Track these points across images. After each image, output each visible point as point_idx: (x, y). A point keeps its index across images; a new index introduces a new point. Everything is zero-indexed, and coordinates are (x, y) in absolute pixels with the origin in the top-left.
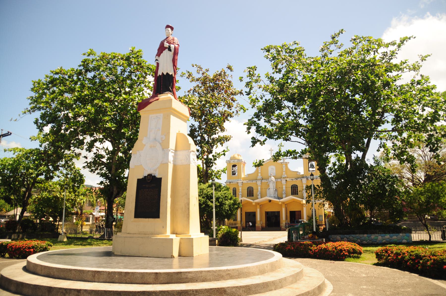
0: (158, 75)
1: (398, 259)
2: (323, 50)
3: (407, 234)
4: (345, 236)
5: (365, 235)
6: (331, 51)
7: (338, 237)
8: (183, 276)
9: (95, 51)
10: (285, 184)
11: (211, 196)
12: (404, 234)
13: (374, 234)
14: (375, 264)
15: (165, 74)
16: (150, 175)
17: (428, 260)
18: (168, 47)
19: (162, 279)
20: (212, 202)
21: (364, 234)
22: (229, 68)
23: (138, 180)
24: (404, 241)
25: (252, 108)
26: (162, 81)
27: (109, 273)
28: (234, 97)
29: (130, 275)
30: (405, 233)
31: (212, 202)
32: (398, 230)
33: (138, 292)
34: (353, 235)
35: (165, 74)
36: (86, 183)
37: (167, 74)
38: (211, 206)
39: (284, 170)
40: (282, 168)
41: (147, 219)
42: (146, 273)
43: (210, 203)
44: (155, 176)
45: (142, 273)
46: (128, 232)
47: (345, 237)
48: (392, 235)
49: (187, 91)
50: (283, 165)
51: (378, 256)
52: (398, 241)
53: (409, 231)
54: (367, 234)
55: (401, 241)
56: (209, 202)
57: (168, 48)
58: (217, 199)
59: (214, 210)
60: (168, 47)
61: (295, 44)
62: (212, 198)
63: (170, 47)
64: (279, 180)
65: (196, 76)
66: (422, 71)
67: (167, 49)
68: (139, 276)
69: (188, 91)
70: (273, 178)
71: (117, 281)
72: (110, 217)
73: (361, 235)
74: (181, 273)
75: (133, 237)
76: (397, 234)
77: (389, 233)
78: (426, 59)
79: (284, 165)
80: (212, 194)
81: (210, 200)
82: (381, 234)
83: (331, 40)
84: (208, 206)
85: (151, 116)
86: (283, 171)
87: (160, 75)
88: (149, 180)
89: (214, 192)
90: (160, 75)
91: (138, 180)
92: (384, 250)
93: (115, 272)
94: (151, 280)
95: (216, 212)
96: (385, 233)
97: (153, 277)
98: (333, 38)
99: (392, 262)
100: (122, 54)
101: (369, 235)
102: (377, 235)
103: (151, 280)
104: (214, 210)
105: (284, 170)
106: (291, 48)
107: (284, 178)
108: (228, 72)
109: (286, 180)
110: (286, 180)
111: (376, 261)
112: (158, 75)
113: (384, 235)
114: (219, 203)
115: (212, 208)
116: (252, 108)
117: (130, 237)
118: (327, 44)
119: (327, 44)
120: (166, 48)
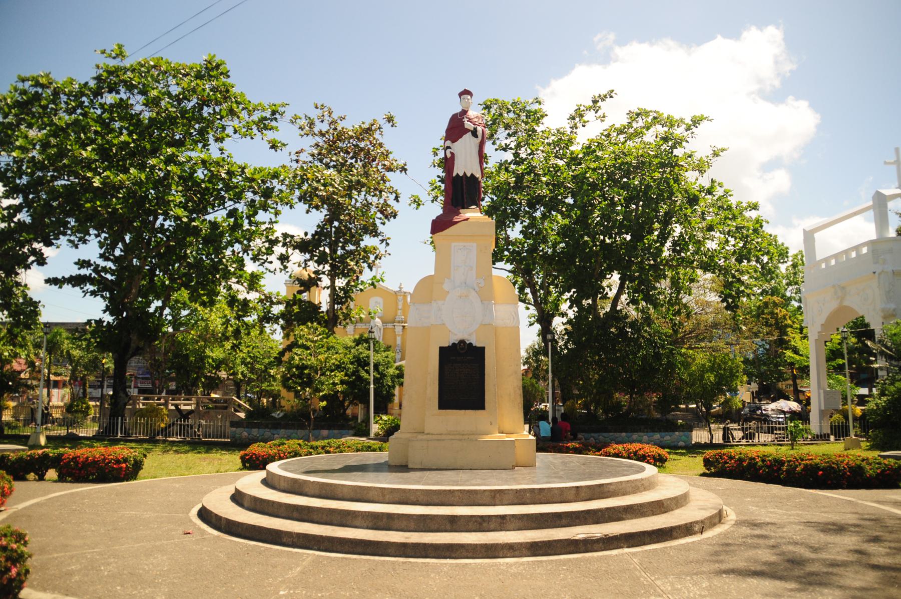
0: (454, 175)
1: (743, 467)
2: (573, 118)
3: (686, 433)
4: (593, 434)
5: (624, 434)
6: (585, 122)
7: (325, 432)
8: (606, 490)
9: (127, 51)
10: (401, 333)
11: (365, 360)
12: (681, 433)
13: (637, 432)
14: (704, 475)
15: (469, 175)
16: (462, 342)
17: (796, 466)
18: (472, 129)
19: (583, 494)
20: (368, 372)
21: (621, 432)
22: (390, 119)
23: (442, 349)
24: (681, 444)
25: (433, 201)
26: (465, 187)
27: (517, 491)
28: (387, 174)
29: (546, 491)
30: (683, 431)
31: (368, 372)
32: (671, 427)
33: (583, 512)
34: (605, 434)
35: (469, 175)
36: (43, 318)
37: (472, 175)
38: (367, 379)
39: (400, 307)
40: (397, 304)
41: (463, 411)
42: (566, 488)
43: (363, 374)
44: (471, 344)
45: (560, 488)
46: (426, 432)
47: (591, 437)
48: (663, 434)
49: (294, 152)
50: (399, 297)
51: (707, 463)
52: (672, 444)
53: (690, 429)
54: (626, 432)
55: (676, 443)
56: (363, 372)
57: (472, 132)
58: (376, 366)
59: (372, 386)
60: (472, 129)
61: (537, 102)
62: (368, 364)
63: (475, 129)
64: (390, 326)
65: (320, 127)
66: (710, 174)
67: (470, 132)
68: (556, 492)
69: (297, 153)
70: (377, 320)
71: (528, 501)
72: (122, 394)
73: (618, 434)
74: (603, 485)
75: (443, 440)
76: (671, 433)
77: (660, 431)
78: (721, 153)
79: (400, 298)
80: (368, 357)
81: (363, 369)
82: (647, 432)
83: (591, 104)
84: (360, 378)
85: (453, 244)
86: (397, 309)
87: (458, 174)
88: (462, 349)
89: (371, 353)
90: (458, 174)
91: (442, 349)
92: (718, 454)
93: (525, 490)
94: (571, 497)
95: (375, 389)
96: (654, 431)
97: (573, 492)
98: (595, 102)
99: (731, 471)
100: (189, 63)
101: (629, 434)
102: (642, 434)
103: (571, 497)
104: (372, 386)
105: (400, 307)
106: (528, 108)
107: (399, 322)
108: (386, 127)
109: (404, 327)
110: (404, 327)
111: (703, 470)
112: (454, 175)
113: (651, 434)
114: (379, 374)
115: (369, 383)
116: (433, 201)
117: (438, 440)
118: (582, 108)
119: (582, 108)
120: (468, 131)
